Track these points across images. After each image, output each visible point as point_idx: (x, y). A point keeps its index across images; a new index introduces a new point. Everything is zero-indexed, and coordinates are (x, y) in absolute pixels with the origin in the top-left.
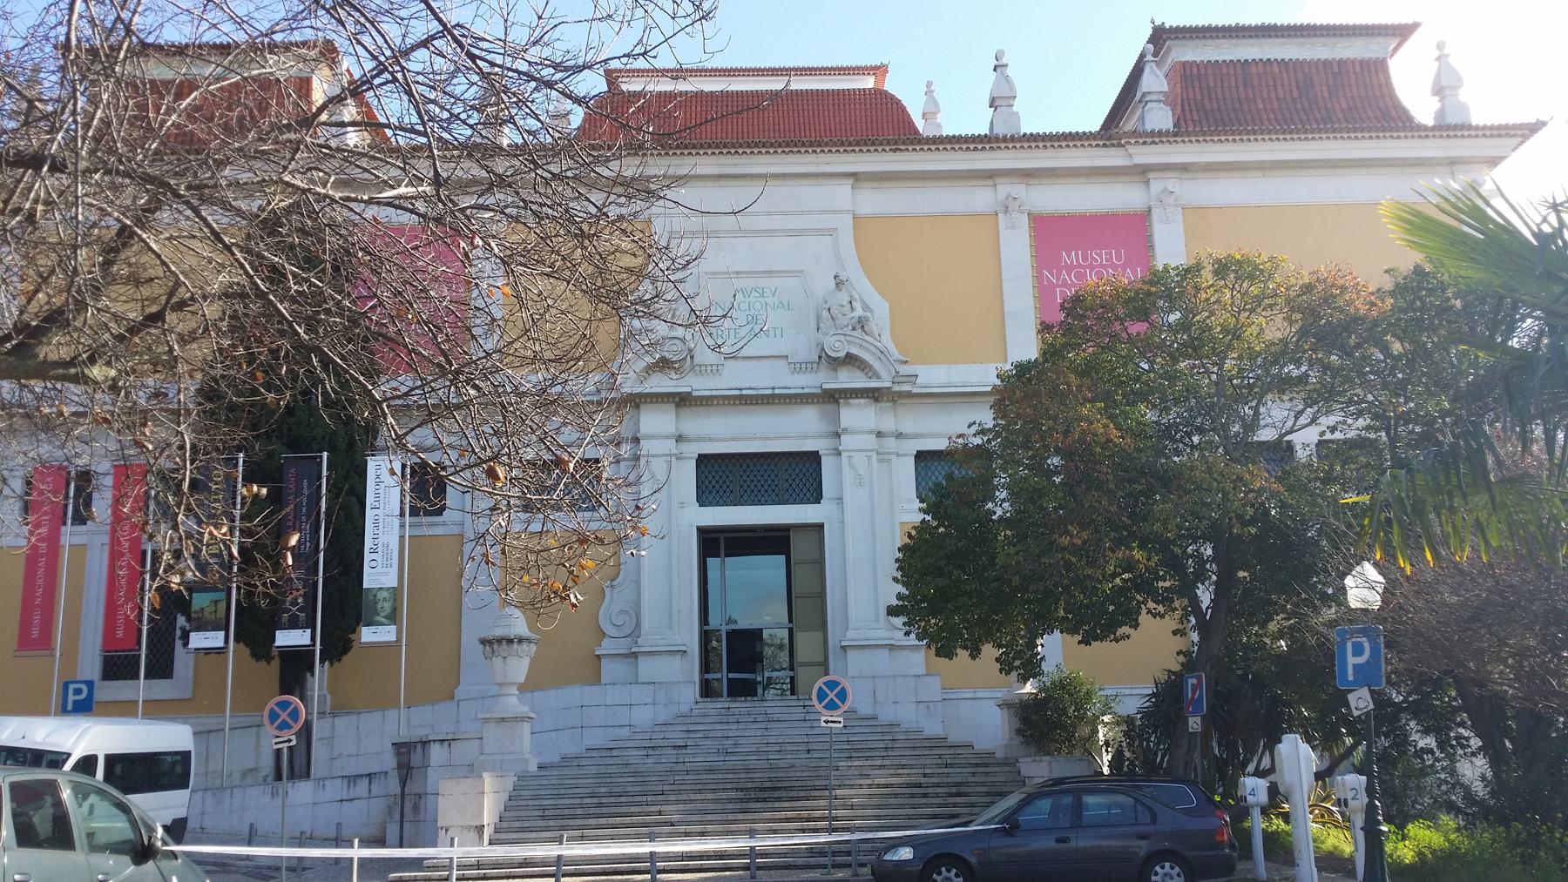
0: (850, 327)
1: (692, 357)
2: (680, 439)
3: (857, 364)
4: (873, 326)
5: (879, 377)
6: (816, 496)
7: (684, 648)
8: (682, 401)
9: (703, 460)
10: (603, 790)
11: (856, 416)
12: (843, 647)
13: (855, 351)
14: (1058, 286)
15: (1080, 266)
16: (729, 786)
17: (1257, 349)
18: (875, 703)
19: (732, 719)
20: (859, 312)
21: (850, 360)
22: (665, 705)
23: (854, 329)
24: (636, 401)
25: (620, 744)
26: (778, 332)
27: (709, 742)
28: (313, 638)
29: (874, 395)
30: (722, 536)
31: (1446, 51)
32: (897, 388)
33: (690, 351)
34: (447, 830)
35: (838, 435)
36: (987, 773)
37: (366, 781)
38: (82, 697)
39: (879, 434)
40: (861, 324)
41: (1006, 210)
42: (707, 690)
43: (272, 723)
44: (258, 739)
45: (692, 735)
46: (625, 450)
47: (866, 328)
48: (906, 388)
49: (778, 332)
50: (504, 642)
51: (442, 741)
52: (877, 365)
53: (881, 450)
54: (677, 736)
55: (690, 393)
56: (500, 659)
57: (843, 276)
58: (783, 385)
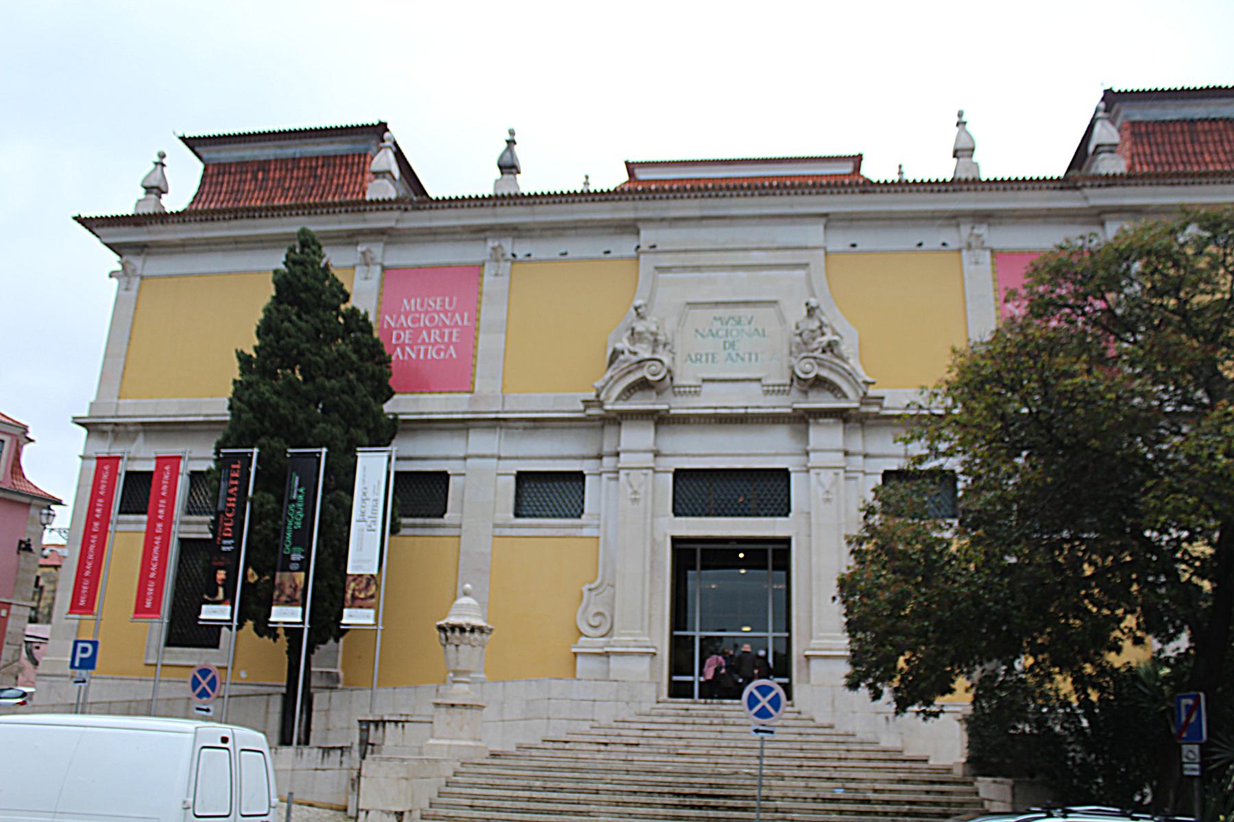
0: (820, 350)
1: (672, 379)
2: (657, 454)
3: (827, 385)
4: (844, 348)
5: (845, 396)
6: (784, 509)
7: (652, 650)
8: (661, 420)
9: (679, 474)
10: (538, 784)
11: (826, 437)
12: (807, 657)
13: (824, 373)
14: (395, 329)
15: (416, 311)
16: (666, 790)
17: (1189, 377)
18: (503, 703)
19: (690, 720)
20: (829, 337)
21: (819, 383)
22: (627, 703)
23: (824, 352)
24: (617, 419)
25: (575, 738)
26: (753, 357)
27: (661, 742)
28: (376, 619)
29: (841, 415)
30: (699, 547)
31: (964, 119)
32: (864, 409)
33: (669, 371)
34: (367, 813)
35: (807, 454)
36: (942, 793)
37: (339, 752)
38: (86, 656)
39: (846, 454)
40: (830, 347)
41: (969, 247)
42: (678, 690)
43: (770, 715)
44: (268, 706)
45: (646, 733)
46: (608, 462)
47: (836, 351)
48: (875, 409)
49: (753, 357)
50: (457, 630)
51: (396, 722)
52: (845, 387)
53: (848, 468)
54: (631, 735)
55: (668, 411)
56: (453, 648)
57: (813, 302)
58: (755, 404)
